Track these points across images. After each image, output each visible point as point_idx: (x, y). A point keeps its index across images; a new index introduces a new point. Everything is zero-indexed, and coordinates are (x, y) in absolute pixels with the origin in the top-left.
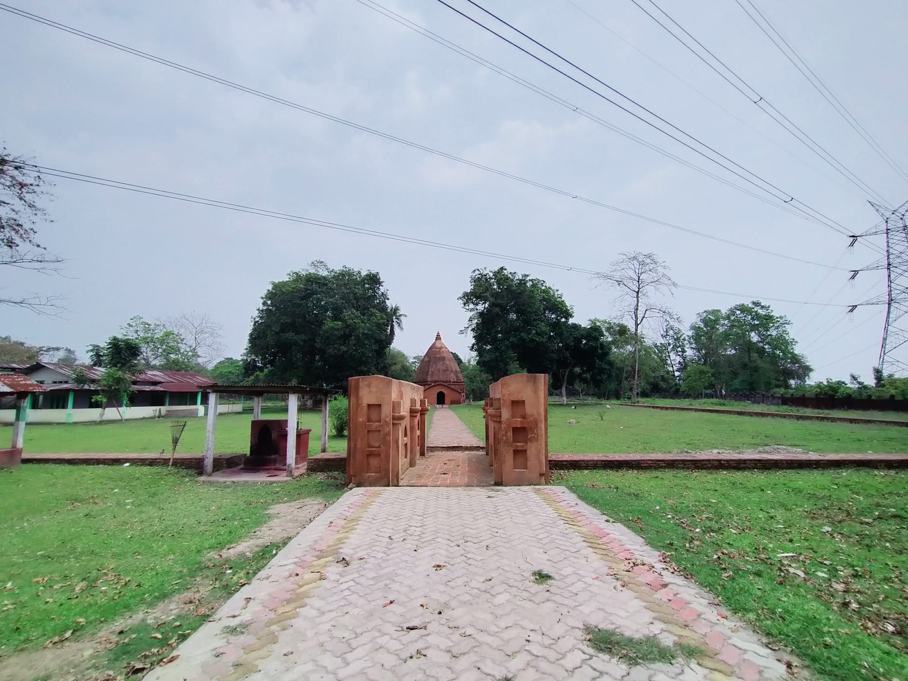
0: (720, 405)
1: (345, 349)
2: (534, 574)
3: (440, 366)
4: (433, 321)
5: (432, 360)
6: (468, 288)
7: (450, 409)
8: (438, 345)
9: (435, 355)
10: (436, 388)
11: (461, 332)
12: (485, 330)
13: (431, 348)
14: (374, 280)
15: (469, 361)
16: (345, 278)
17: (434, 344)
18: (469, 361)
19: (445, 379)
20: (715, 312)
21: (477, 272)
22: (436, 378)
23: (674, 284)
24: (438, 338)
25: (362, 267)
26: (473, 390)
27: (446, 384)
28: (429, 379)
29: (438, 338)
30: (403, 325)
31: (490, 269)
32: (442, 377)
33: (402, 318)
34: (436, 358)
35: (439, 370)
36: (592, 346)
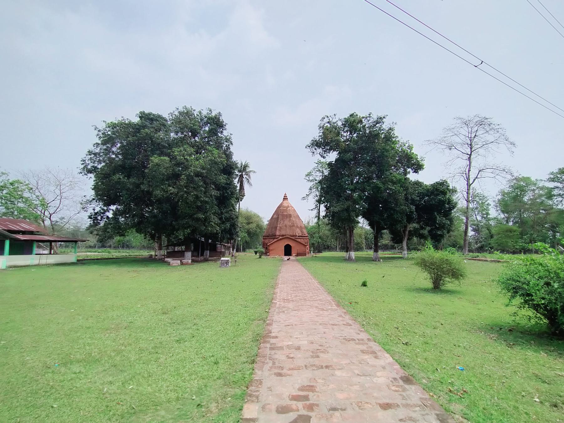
0: (89, 252)
1: (175, 190)
2: (220, 113)
3: (287, 222)
4: (280, 181)
5: (280, 217)
6: (317, 134)
7: (297, 260)
8: (285, 204)
9: (282, 214)
10: (283, 241)
11: (304, 198)
12: (331, 188)
13: (279, 207)
14: (216, 124)
15: (308, 223)
16: (187, 123)
17: (281, 204)
18: (308, 223)
19: (291, 234)
20: (527, 180)
21: (326, 120)
22: (283, 233)
23: (513, 144)
24: (285, 198)
25: (202, 105)
26: (313, 244)
27: (293, 238)
28: (278, 233)
29: (285, 198)
30: (251, 181)
31: (340, 116)
32: (288, 232)
33: (251, 174)
34: (283, 215)
35: (286, 226)
36: (440, 200)
